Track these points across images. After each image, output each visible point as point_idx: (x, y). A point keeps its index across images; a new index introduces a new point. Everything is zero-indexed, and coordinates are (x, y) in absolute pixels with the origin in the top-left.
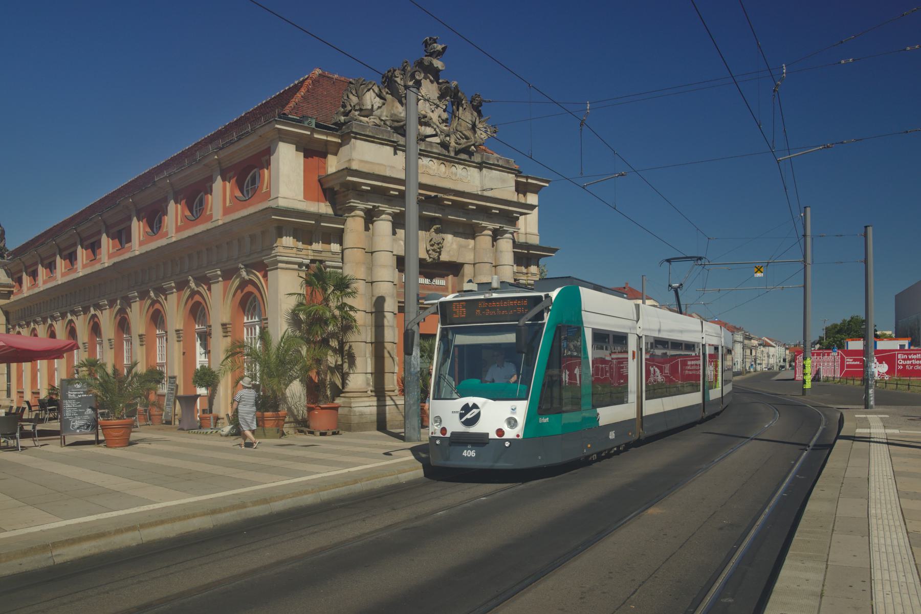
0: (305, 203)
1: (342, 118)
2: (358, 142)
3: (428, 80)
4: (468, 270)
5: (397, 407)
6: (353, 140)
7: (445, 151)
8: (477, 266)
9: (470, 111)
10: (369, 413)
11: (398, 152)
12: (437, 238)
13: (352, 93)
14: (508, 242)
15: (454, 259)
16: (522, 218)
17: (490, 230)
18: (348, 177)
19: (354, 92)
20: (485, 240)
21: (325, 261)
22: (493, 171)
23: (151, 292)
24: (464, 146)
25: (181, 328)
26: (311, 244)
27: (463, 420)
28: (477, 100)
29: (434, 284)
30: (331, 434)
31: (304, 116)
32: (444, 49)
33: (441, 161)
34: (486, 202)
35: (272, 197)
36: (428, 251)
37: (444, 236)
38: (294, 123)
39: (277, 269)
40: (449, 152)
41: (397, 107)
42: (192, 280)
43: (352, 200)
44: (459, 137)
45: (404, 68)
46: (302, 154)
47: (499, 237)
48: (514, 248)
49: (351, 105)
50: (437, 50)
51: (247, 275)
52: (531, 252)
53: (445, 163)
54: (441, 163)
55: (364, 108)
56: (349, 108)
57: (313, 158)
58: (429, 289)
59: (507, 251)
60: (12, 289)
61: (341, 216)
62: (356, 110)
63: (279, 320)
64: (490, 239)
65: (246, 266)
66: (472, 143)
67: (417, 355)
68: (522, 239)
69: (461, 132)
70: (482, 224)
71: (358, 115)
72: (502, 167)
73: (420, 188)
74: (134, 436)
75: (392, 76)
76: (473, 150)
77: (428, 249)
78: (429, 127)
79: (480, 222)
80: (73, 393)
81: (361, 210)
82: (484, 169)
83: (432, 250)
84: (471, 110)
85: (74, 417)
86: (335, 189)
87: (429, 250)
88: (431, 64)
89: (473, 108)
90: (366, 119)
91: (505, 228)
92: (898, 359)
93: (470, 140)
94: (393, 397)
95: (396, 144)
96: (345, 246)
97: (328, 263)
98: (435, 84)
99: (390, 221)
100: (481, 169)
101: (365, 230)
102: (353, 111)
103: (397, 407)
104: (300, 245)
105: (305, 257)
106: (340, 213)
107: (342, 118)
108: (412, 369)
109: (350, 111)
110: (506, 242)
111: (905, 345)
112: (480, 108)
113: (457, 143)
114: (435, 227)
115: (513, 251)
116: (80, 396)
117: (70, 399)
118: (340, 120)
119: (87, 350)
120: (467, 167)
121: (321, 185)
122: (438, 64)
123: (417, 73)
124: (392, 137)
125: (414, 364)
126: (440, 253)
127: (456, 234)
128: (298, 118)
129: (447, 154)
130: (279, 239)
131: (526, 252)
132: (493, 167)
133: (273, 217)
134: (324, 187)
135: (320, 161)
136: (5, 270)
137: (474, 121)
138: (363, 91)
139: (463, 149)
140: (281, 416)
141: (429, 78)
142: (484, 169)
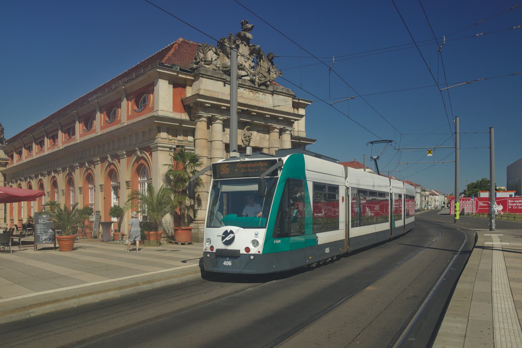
0: (173, 113)
1: (195, 66)
2: (204, 79)
3: (243, 44)
11: (226, 85)
13: (200, 52)
14: (288, 136)
16: (296, 122)
17: (278, 129)
19: (201, 51)
20: (275, 135)
22: (280, 96)
23: (86, 163)
24: (263, 82)
25: (103, 184)
26: (177, 137)
27: (224, 241)
30: (187, 244)
32: (252, 27)
33: (250, 90)
35: (155, 110)
36: (243, 141)
37: (252, 132)
38: (168, 68)
39: (157, 150)
40: (255, 85)
41: (226, 60)
43: (200, 112)
44: (260, 76)
45: (230, 37)
46: (172, 86)
47: (283, 133)
49: (200, 58)
51: (141, 154)
52: (301, 141)
53: (253, 91)
56: (199, 60)
57: (178, 88)
60: (8, 162)
61: (194, 121)
62: (202, 61)
66: (268, 80)
69: (261, 74)
70: (273, 126)
71: (204, 64)
74: (76, 245)
75: (223, 42)
77: (243, 140)
78: (244, 71)
79: (273, 125)
80: (42, 220)
82: (275, 95)
85: (42, 234)
86: (191, 106)
87: (244, 140)
88: (245, 35)
89: (268, 60)
91: (286, 128)
92: (508, 203)
95: (225, 81)
97: (186, 147)
99: (278, 132)
100: (273, 95)
102: (201, 62)
104: (170, 137)
105: (173, 144)
106: (193, 119)
107: (195, 66)
109: (199, 62)
110: (287, 136)
111: (512, 195)
112: (273, 60)
113: (259, 80)
114: (247, 127)
115: (291, 141)
117: (40, 224)
118: (193, 67)
119: (50, 196)
120: (265, 94)
121: (183, 104)
122: (249, 35)
127: (258, 131)
128: (170, 66)
129: (254, 86)
131: (298, 141)
132: (280, 93)
133: (155, 121)
134: (184, 105)
136: (4, 151)
138: (206, 50)
140: (159, 233)
141: (244, 43)
142: (275, 95)
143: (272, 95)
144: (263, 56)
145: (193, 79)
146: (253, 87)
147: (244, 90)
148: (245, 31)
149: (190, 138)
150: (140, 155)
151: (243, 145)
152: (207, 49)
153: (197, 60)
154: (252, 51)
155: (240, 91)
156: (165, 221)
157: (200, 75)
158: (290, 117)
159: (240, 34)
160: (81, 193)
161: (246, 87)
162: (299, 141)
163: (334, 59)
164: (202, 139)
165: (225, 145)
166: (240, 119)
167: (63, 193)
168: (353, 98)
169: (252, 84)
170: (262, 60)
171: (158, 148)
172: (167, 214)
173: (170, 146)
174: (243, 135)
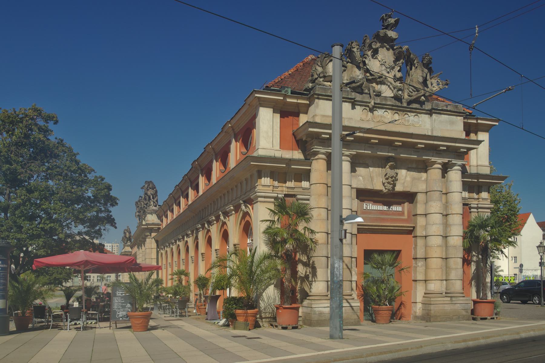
0: (281, 152)
1: (310, 85)
2: (321, 101)
3: (385, 48)
4: (420, 198)
5: (353, 309)
6: (316, 100)
7: (398, 103)
8: (428, 193)
9: (420, 69)
10: (327, 313)
11: (356, 107)
12: (391, 173)
13: (318, 65)
14: (457, 173)
15: (408, 189)
16: (472, 153)
17: (439, 164)
18: (309, 129)
19: (319, 64)
20: (435, 173)
21: (470, 204)
22: (443, 116)
23: (206, 224)
24: (415, 97)
25: (218, 248)
26: (285, 182)
28: (426, 59)
29: (391, 210)
30: (291, 328)
31: (281, 87)
32: (397, 22)
33: (395, 111)
34: (433, 141)
35: (256, 149)
36: (384, 184)
37: (397, 171)
38: (270, 91)
39: (257, 202)
40: (401, 103)
41: (355, 72)
42: (221, 214)
43: (316, 147)
45: (364, 41)
46: (278, 116)
47: (449, 170)
48: (462, 178)
49: (317, 74)
50: (391, 23)
51: (246, 208)
52: (480, 180)
53: (398, 112)
54: (395, 113)
55: (327, 75)
56: (316, 76)
57: (288, 117)
58: (387, 214)
59: (456, 181)
60: (160, 227)
61: (309, 160)
62: (321, 78)
63: (258, 240)
64: (440, 172)
65: (245, 202)
66: (421, 94)
67: (340, 266)
68: (473, 171)
70: (431, 159)
71: (323, 81)
72: (450, 111)
73: (344, 130)
74: (152, 323)
75: (350, 48)
76: (423, 99)
77: (384, 182)
78: (384, 85)
79: (430, 158)
80: (120, 292)
81: (323, 154)
82: (433, 114)
83: (387, 182)
84: (421, 68)
85: (119, 309)
86: (304, 139)
87: (385, 183)
88: (386, 35)
89: (423, 66)
90: (329, 83)
91: (453, 162)
93: (420, 92)
94: (348, 300)
95: (353, 101)
96: (312, 182)
97: (299, 197)
98: (391, 51)
100: (431, 115)
101: (442, 178)
102: (319, 79)
103: (353, 309)
104: (276, 183)
105: (280, 192)
106: (308, 157)
107: (310, 85)
108: (335, 279)
109: (316, 79)
110: (455, 173)
112: (430, 66)
113: (409, 96)
114: (389, 164)
115: (462, 181)
116: (124, 295)
117: (118, 297)
118: (308, 87)
119: (184, 264)
121: (295, 138)
122: (392, 34)
123: (373, 43)
124: (350, 95)
125: (336, 275)
126: (394, 185)
127: (409, 169)
128: (279, 89)
129: (400, 104)
130: (259, 180)
131: (476, 180)
132: (442, 112)
133: (252, 163)
134: (297, 139)
135: (294, 119)
136: (157, 215)
137: (425, 75)
138: (326, 62)
139: (414, 99)
140: (249, 313)
141: (385, 46)
142: (433, 114)
143: (430, 116)
144: (415, 60)
145: (307, 104)
146: (398, 106)
147: (385, 111)
148: (386, 29)
149: (305, 184)
150: (245, 210)
151: (383, 188)
152: (327, 59)
153: (313, 77)
154: (398, 55)
155: (378, 114)
156: (267, 296)
157: (315, 96)
158: (457, 145)
159: (378, 34)
160: (203, 260)
161: (387, 107)
162: (478, 180)
163: (477, 29)
164: (318, 184)
165: (357, 190)
166: (378, 153)
167: (192, 261)
168: (510, 89)
169: (397, 102)
170: (413, 68)
171: (258, 199)
172: (270, 287)
173: (275, 195)
174: (384, 176)
